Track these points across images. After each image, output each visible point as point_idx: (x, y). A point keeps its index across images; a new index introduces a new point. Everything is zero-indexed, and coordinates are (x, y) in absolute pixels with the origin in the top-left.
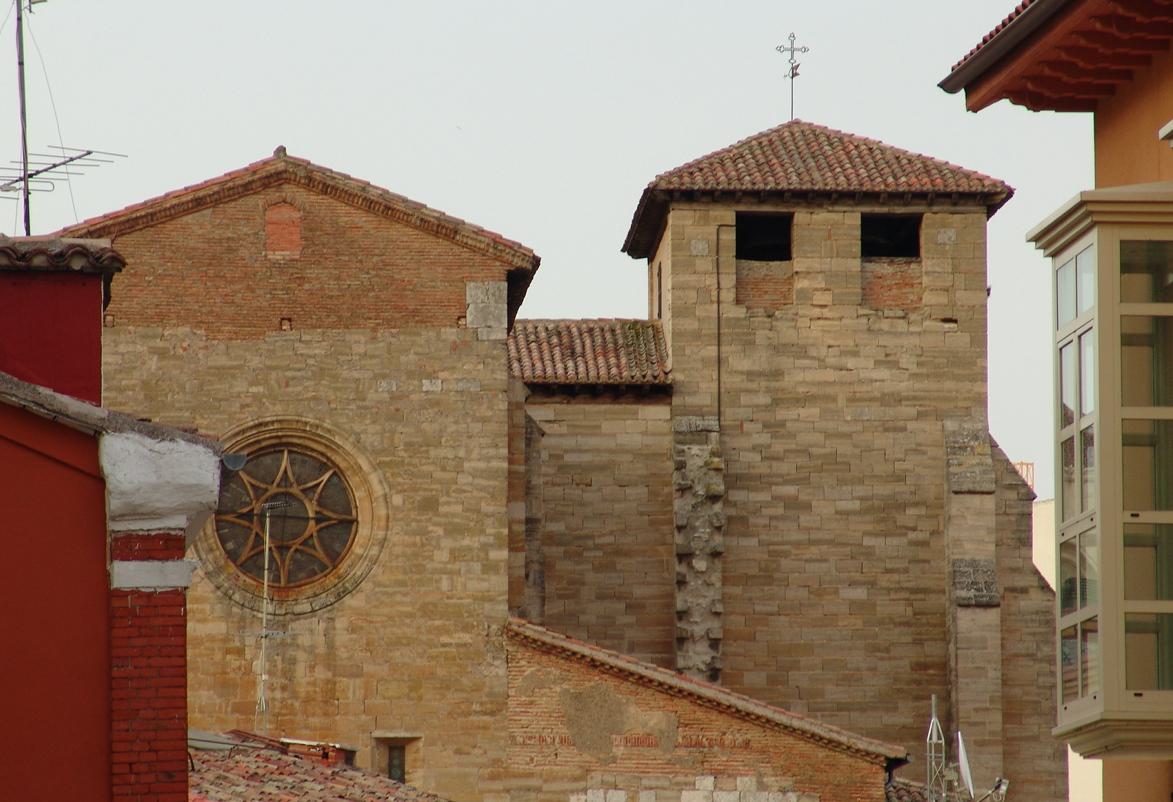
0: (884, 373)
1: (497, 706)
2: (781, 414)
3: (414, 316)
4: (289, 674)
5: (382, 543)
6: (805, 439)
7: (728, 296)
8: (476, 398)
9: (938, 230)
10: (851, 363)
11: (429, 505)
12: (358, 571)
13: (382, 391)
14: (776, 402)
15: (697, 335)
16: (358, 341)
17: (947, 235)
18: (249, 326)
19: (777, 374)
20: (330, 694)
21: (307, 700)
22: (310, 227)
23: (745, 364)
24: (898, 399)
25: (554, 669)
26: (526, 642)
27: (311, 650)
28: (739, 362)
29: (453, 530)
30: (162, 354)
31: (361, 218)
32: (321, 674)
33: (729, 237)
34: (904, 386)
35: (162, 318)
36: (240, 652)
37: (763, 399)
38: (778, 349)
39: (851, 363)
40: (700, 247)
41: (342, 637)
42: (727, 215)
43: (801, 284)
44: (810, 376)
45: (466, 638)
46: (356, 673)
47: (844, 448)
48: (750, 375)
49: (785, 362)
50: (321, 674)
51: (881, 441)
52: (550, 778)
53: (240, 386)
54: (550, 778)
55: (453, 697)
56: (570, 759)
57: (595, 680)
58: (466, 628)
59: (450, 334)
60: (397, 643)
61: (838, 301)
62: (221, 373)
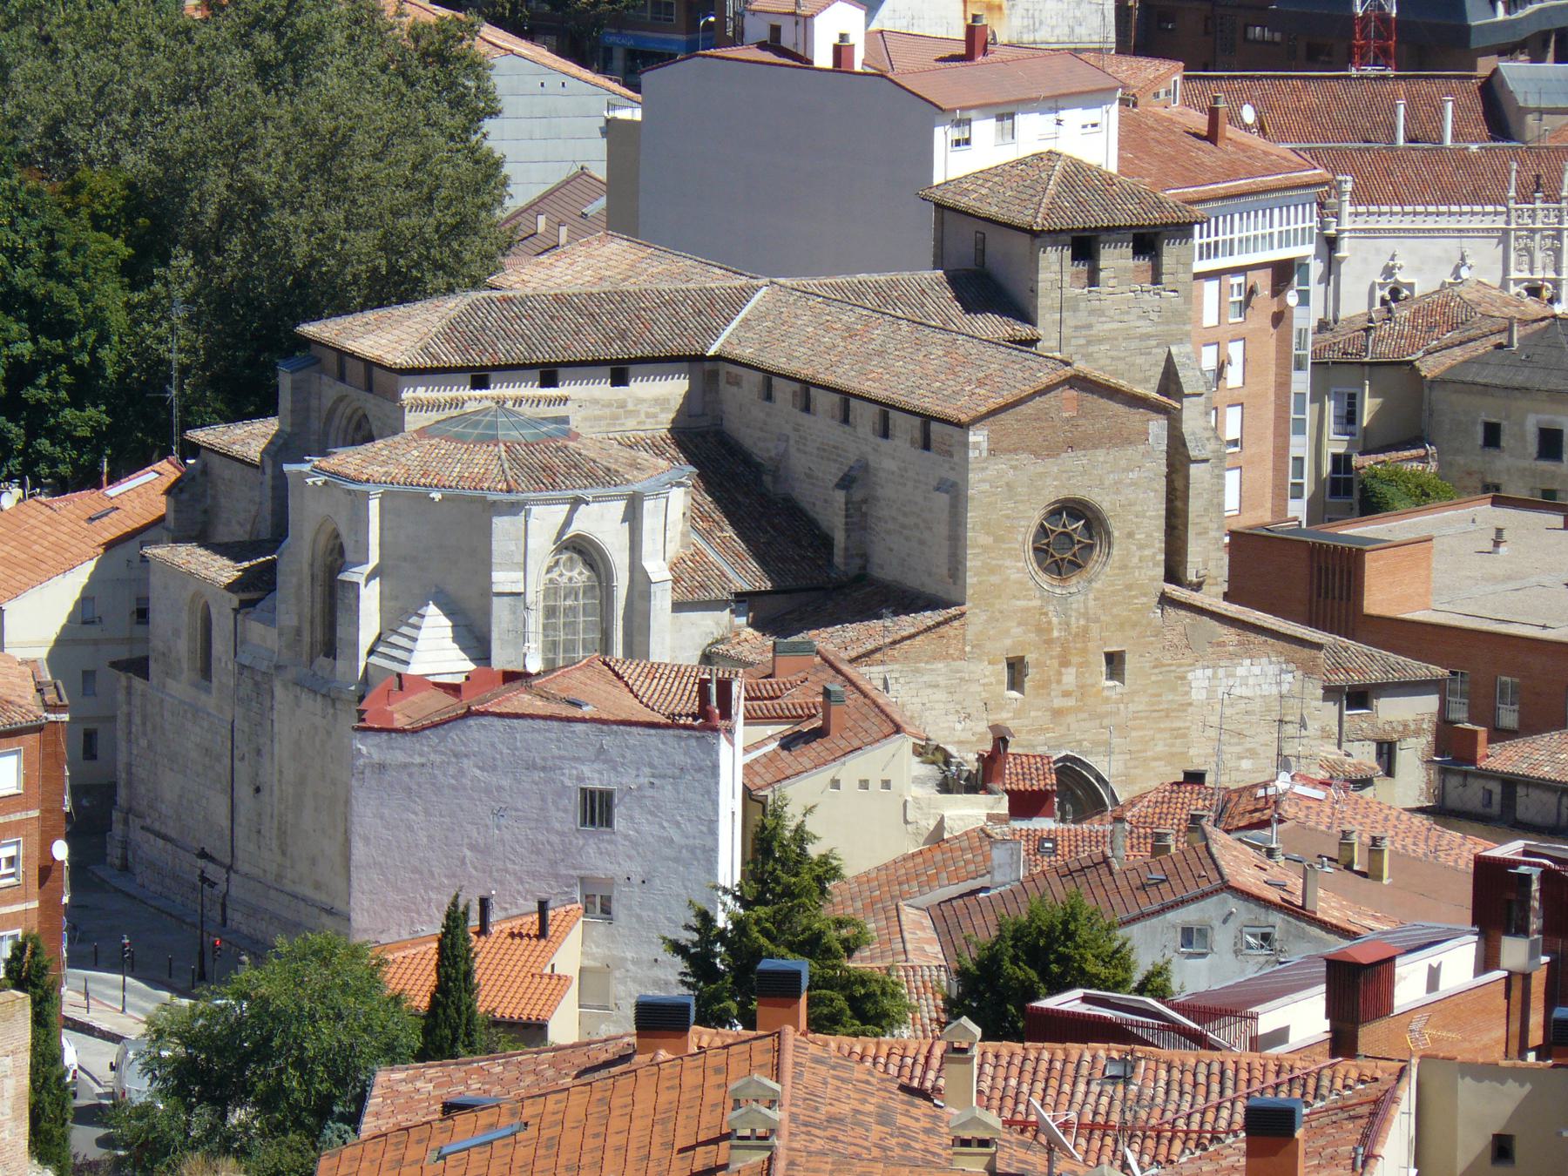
2: (1091, 349)
3: (1128, 441)
6: (1102, 362)
8: (1151, 480)
10: (1126, 318)
14: (1089, 343)
16: (1100, 455)
18: (1052, 451)
19: (1089, 326)
20: (1086, 630)
21: (1077, 635)
24: (1148, 337)
27: (1077, 610)
29: (1141, 547)
30: (1014, 468)
32: (1082, 622)
35: (1015, 451)
36: (1046, 614)
37: (1082, 341)
38: (1092, 312)
39: (1126, 318)
41: (1091, 603)
44: (1106, 327)
45: (1145, 600)
46: (1097, 620)
47: (1121, 366)
48: (1077, 328)
49: (1093, 319)
50: (1082, 622)
51: (1140, 360)
52: (1180, 666)
53: (1049, 481)
58: (1145, 595)
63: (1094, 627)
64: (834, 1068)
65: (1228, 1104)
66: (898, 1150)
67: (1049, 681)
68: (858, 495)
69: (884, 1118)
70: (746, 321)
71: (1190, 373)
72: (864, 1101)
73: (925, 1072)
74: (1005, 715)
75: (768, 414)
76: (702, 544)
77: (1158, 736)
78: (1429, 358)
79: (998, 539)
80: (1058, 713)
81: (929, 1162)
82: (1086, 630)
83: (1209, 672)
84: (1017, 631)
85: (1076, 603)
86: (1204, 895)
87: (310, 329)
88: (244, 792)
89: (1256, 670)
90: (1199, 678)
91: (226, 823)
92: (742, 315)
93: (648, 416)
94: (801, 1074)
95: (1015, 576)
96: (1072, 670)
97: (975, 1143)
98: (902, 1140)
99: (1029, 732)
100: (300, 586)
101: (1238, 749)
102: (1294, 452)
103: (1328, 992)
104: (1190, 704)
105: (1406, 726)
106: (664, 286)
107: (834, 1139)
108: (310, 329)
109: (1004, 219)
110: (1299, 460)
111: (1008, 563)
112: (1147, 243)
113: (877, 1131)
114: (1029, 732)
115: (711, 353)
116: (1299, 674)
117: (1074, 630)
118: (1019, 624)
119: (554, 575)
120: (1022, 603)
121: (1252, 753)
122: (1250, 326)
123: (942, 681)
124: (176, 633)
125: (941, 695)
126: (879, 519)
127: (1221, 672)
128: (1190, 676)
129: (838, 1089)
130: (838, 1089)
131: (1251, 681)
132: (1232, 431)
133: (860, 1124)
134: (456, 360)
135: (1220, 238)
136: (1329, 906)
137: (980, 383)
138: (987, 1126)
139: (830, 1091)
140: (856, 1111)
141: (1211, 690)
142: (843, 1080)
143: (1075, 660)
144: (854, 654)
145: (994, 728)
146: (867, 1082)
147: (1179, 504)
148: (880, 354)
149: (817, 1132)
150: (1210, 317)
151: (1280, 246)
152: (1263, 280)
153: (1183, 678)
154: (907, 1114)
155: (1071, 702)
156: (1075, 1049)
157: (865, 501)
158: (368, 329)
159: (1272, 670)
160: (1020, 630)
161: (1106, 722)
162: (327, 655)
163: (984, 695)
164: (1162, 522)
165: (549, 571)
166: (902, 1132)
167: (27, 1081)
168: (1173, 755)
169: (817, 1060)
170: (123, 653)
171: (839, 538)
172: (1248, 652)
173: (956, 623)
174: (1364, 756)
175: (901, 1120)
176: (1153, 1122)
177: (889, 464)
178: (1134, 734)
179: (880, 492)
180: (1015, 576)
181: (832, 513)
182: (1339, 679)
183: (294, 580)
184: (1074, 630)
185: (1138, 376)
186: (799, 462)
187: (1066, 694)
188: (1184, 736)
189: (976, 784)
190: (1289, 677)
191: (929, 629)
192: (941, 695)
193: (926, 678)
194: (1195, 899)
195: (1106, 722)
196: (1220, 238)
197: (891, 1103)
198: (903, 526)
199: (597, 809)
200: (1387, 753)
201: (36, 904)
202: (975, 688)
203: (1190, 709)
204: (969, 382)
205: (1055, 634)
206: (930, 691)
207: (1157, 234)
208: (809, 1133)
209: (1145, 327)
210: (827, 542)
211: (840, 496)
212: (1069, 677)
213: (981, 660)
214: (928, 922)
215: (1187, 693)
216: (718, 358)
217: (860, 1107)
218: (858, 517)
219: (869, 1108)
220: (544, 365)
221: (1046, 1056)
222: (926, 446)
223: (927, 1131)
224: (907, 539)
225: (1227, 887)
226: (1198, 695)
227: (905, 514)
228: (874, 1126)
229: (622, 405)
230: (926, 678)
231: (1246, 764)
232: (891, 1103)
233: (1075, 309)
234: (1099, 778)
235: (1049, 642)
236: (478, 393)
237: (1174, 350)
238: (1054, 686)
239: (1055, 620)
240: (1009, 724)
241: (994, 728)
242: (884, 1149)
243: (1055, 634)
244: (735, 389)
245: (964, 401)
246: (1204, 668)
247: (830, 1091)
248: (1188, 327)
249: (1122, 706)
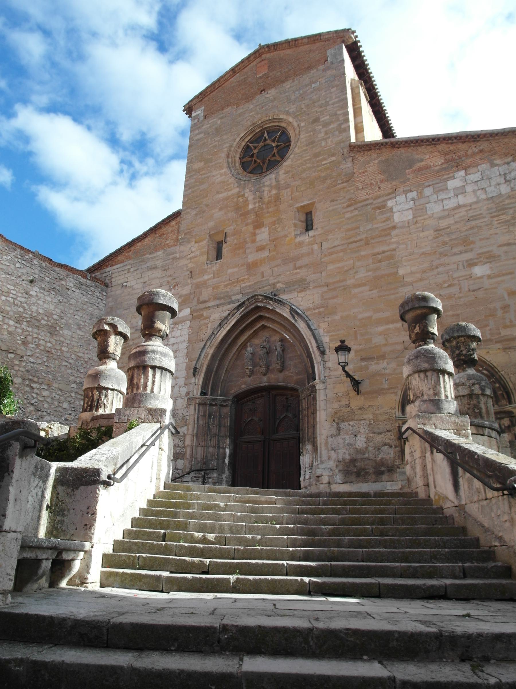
20: (277, 198)
21: (269, 202)
32: (274, 192)
58: (333, 155)
63: (286, 194)
67: (245, 242)
77: (358, 264)
80: (252, 267)
82: (277, 198)
83: (414, 194)
84: (218, 214)
89: (474, 177)
90: (401, 208)
99: (226, 286)
100: (388, 225)
104: (394, 227)
106: (241, 78)
114: (226, 286)
117: (266, 200)
118: (221, 209)
123: (159, 263)
125: (158, 273)
128: (390, 204)
131: (469, 189)
143: (268, 220)
153: (382, 207)
161: (299, 263)
163: (190, 266)
173: (173, 223)
178: (330, 267)
184: (266, 200)
187: (261, 249)
188: (391, 257)
193: (148, 265)
195: (299, 263)
203: (394, 233)
205: (251, 206)
206: (150, 273)
212: (263, 235)
213: (189, 242)
230: (148, 265)
234: (293, 312)
235: (245, 214)
238: (249, 245)
246: (406, 192)
249: (316, 247)
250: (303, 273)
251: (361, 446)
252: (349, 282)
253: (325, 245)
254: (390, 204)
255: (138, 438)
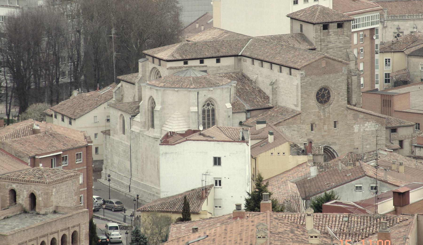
0: (340, 44)
1: (346, 116)
2: (328, 50)
4: (325, 115)
5: (334, 99)
7: (322, 36)
9: (346, 25)
11: (339, 94)
12: (331, 102)
13: (334, 81)
14: (328, 49)
15: (318, 41)
17: (347, 25)
19: (327, 45)
20: (329, 116)
22: (327, 63)
23: (324, 45)
24: (341, 47)
25: (352, 111)
26: (349, 109)
28: (323, 44)
29: (341, 96)
30: (311, 79)
31: (332, 61)
33: (322, 28)
34: (341, 45)
35: (311, 75)
37: (326, 49)
38: (328, 42)
40: (319, 30)
41: (330, 110)
42: (322, 25)
43: (330, 33)
44: (331, 45)
47: (335, 54)
48: (325, 46)
49: (328, 44)
50: (328, 114)
51: (340, 53)
53: (319, 82)
54: (352, 124)
55: (342, 116)
56: (354, 122)
57: (356, 112)
59: (341, 73)
60: (336, 110)
61: (334, 35)
62: (317, 80)
63: (331, 116)
64: (279, 220)
65: (372, 226)
66: (296, 239)
68: (275, 87)
69: (292, 232)
70: (247, 46)
71: (352, 56)
72: (287, 228)
73: (300, 221)
74: (311, 137)
75: (253, 68)
76: (239, 99)
78: (407, 50)
79: (308, 95)
80: (323, 136)
81: (303, 242)
83: (359, 125)
84: (313, 117)
85: (327, 110)
86: (360, 177)
87: (145, 52)
88: (133, 160)
89: (370, 124)
90: (356, 128)
91: (130, 168)
92: (246, 45)
93: (225, 69)
94: (272, 222)
95: (312, 104)
96: (326, 126)
97: (314, 237)
98: (296, 237)
100: (145, 112)
101: (366, 143)
102: (376, 73)
103: (393, 199)
105: (406, 137)
107: (281, 237)
108: (145, 52)
109: (307, 21)
110: (377, 75)
111: (310, 101)
112: (340, 25)
113: (291, 235)
115: (240, 54)
116: (380, 125)
119: (204, 107)
120: (313, 110)
121: (369, 144)
122: (365, 44)
123: (296, 129)
124: (117, 124)
125: (296, 132)
126: (280, 92)
127: (361, 125)
128: (354, 126)
129: (281, 225)
130: (281, 225)
131: (369, 127)
132: (361, 68)
133: (287, 233)
134: (180, 58)
135: (357, 23)
136: (390, 179)
137: (303, 59)
138: (316, 233)
139: (279, 226)
140: (286, 230)
141: (359, 130)
142: (282, 223)
144: (275, 123)
145: (308, 140)
146: (287, 223)
147: (350, 86)
148: (279, 53)
149: (276, 235)
150: (355, 41)
151: (371, 25)
152: (368, 34)
154: (297, 230)
155: (326, 133)
156: (335, 214)
157: (276, 88)
158: (159, 51)
159: (374, 124)
160: (314, 117)
161: (335, 138)
162: (152, 128)
164: (346, 90)
165: (204, 106)
166: (296, 235)
167: (88, 230)
168: (350, 145)
169: (276, 219)
170: (104, 129)
171: (271, 97)
172: (367, 120)
173: (299, 116)
174: (396, 145)
175: (296, 232)
176: (355, 231)
177: (282, 79)
179: (280, 86)
180: (312, 104)
181: (268, 92)
182: (389, 126)
183: (144, 111)
185: (339, 57)
186: (260, 79)
187: (325, 131)
189: (304, 152)
190: (377, 126)
191: (292, 117)
192: (296, 132)
193: (292, 129)
194: (358, 178)
195: (335, 138)
196: (357, 23)
197: (293, 228)
198: (285, 93)
199: (217, 161)
200: (401, 143)
201: (86, 189)
202: (303, 130)
204: (300, 59)
205: (322, 117)
206: (293, 132)
207: (343, 23)
208: (274, 236)
209: (341, 45)
210: (268, 98)
211: (271, 87)
212: (326, 127)
213: (305, 124)
214: (295, 185)
215: (354, 130)
216: (241, 56)
217: (286, 229)
218: (274, 91)
219: (288, 229)
220: (201, 58)
221: (328, 216)
222: (291, 74)
223: (302, 235)
224: (287, 96)
225: (366, 175)
226: (356, 131)
227: (286, 91)
228: (290, 234)
229: (219, 67)
230: (292, 129)
231: (368, 147)
232: (293, 228)
233: (324, 41)
234: (334, 150)
235: (321, 119)
236: (185, 65)
237: (348, 50)
239: (322, 114)
240: (312, 139)
241: (308, 140)
242: (292, 239)
243: (322, 117)
244: (245, 63)
245: (299, 64)
247: (279, 226)
248: (351, 45)
250: (335, 141)
251: (314, 175)
252: (345, 145)
253: (340, 134)
254: (354, 126)
255: (103, 172)
